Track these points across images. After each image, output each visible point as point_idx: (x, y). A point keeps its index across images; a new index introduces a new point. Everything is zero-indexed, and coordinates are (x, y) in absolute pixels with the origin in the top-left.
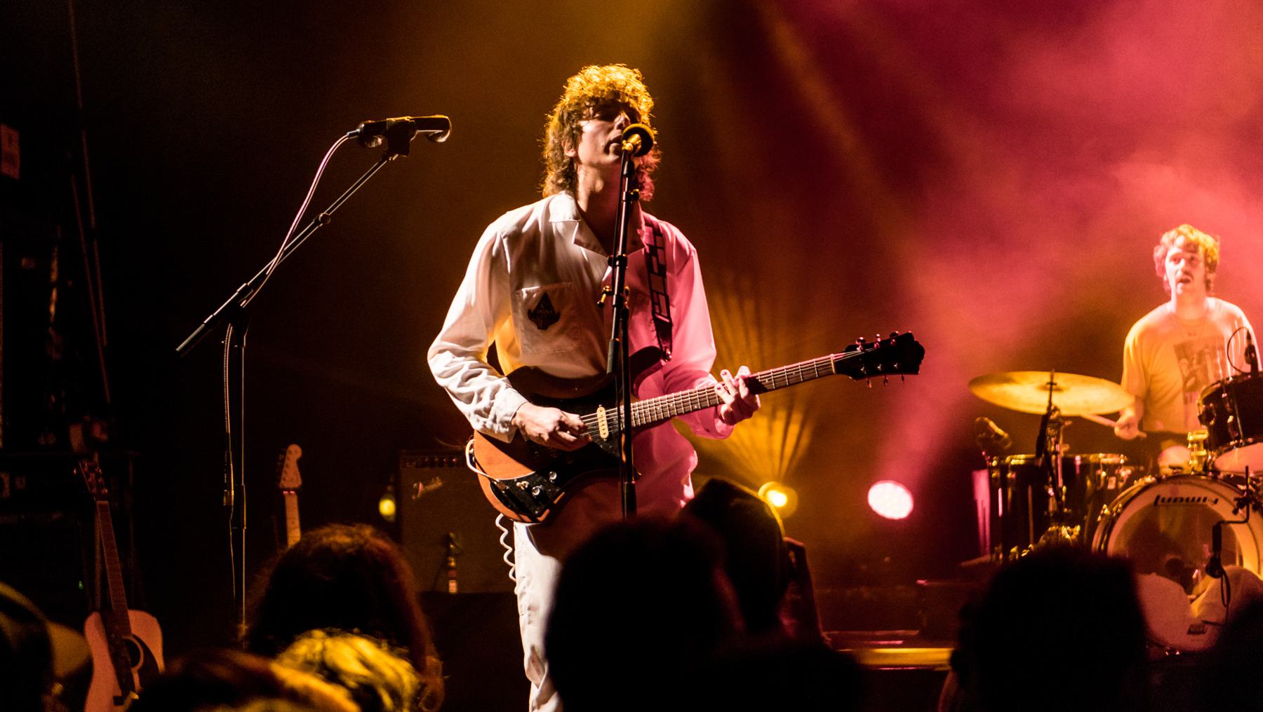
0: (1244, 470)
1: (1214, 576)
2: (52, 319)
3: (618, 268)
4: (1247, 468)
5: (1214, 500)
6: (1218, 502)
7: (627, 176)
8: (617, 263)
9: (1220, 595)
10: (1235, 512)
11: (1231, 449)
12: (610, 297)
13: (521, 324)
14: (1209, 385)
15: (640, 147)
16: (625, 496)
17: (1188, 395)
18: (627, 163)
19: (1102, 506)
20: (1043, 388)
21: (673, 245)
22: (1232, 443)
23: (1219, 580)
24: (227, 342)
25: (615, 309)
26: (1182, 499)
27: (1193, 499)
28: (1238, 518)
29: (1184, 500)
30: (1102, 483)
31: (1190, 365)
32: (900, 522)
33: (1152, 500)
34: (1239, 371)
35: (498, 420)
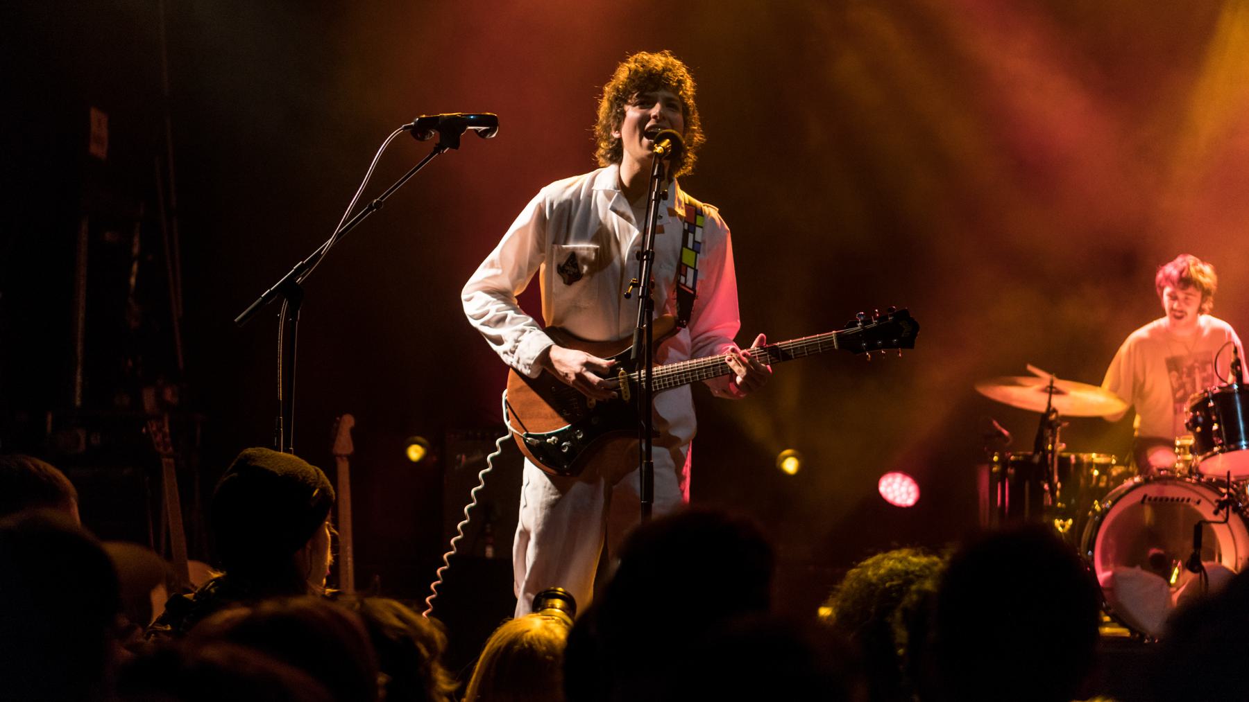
5: (1197, 500)
7: (656, 177)
8: (645, 257)
10: (1216, 513)
11: (1215, 454)
12: (637, 289)
18: (657, 165)
19: (1093, 502)
20: (1044, 391)
22: (1216, 449)
23: (1198, 575)
24: (282, 315)
28: (1219, 518)
30: (1094, 482)
31: (1180, 377)
35: (521, 362)
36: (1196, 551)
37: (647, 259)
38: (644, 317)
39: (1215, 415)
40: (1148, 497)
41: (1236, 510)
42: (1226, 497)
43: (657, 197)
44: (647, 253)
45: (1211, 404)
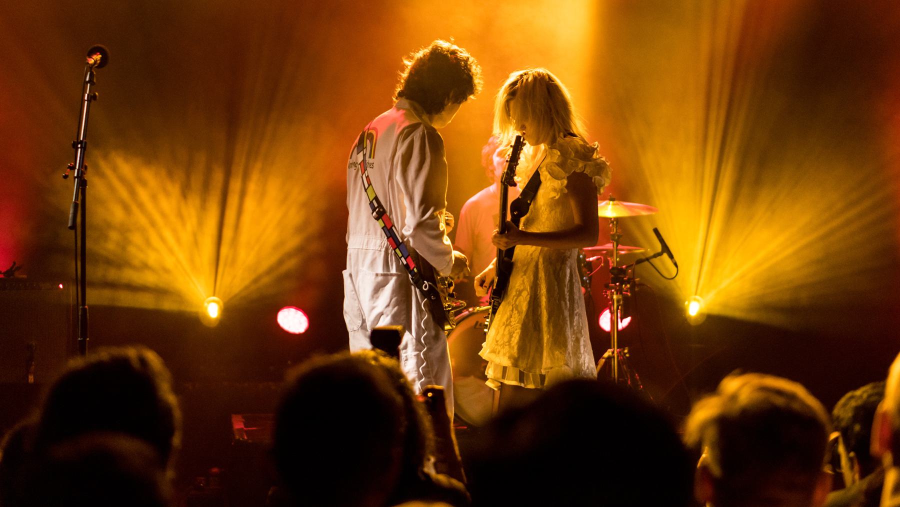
3: (79, 150)
7: (89, 82)
8: (79, 146)
12: (72, 171)
13: (550, 344)
15: (98, 62)
16: (80, 317)
18: (89, 73)
25: (76, 179)
32: (300, 335)
33: (474, 323)
36: (578, 362)
37: (81, 148)
38: (78, 195)
40: (479, 324)
43: (89, 99)
44: (81, 142)
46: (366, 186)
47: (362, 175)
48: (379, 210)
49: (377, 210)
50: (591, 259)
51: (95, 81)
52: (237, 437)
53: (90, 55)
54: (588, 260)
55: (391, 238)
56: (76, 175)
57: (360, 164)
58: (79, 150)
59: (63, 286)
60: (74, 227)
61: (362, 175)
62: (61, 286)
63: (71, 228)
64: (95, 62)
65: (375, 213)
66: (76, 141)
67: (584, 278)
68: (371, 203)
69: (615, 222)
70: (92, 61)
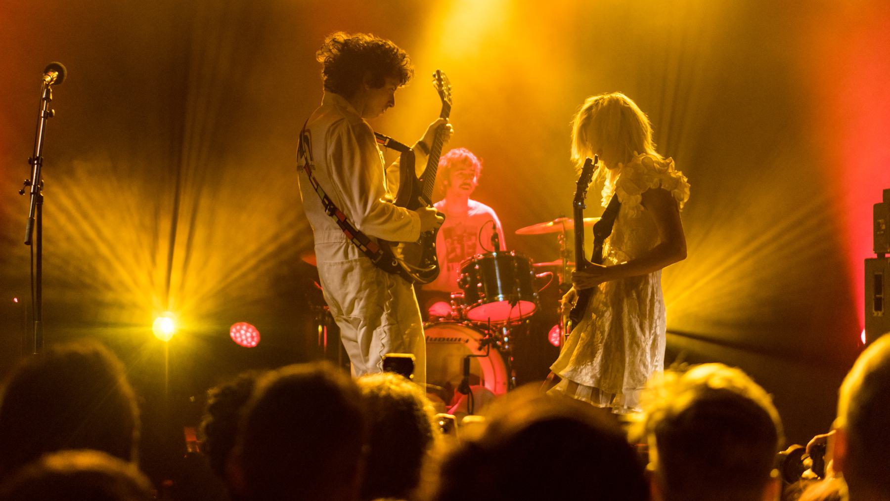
0: (487, 319)
1: (464, 393)
2: (54, 115)
3: (36, 166)
4: (489, 319)
6: (469, 342)
8: (36, 162)
9: (43, 262)
10: (480, 349)
11: (479, 305)
12: (29, 187)
14: (465, 261)
15: (55, 79)
17: (450, 264)
18: (45, 90)
21: (304, 140)
22: (480, 301)
23: (466, 396)
25: (33, 195)
26: (444, 339)
27: (452, 339)
29: (457, 340)
31: (453, 243)
34: (486, 250)
39: (480, 275)
40: (429, 339)
41: (495, 346)
42: (487, 336)
43: (46, 116)
44: (37, 159)
45: (477, 267)
46: (316, 186)
47: (310, 177)
48: (330, 207)
49: (328, 207)
50: (541, 275)
51: (51, 97)
52: (190, 450)
53: (46, 72)
54: (537, 275)
55: (346, 231)
56: (32, 191)
57: (305, 167)
58: (36, 166)
59: (18, 300)
60: (29, 242)
61: (310, 177)
62: (16, 300)
63: (27, 243)
64: (52, 80)
65: (327, 211)
66: (32, 158)
67: (534, 294)
68: (323, 202)
69: (565, 239)
70: (48, 79)
